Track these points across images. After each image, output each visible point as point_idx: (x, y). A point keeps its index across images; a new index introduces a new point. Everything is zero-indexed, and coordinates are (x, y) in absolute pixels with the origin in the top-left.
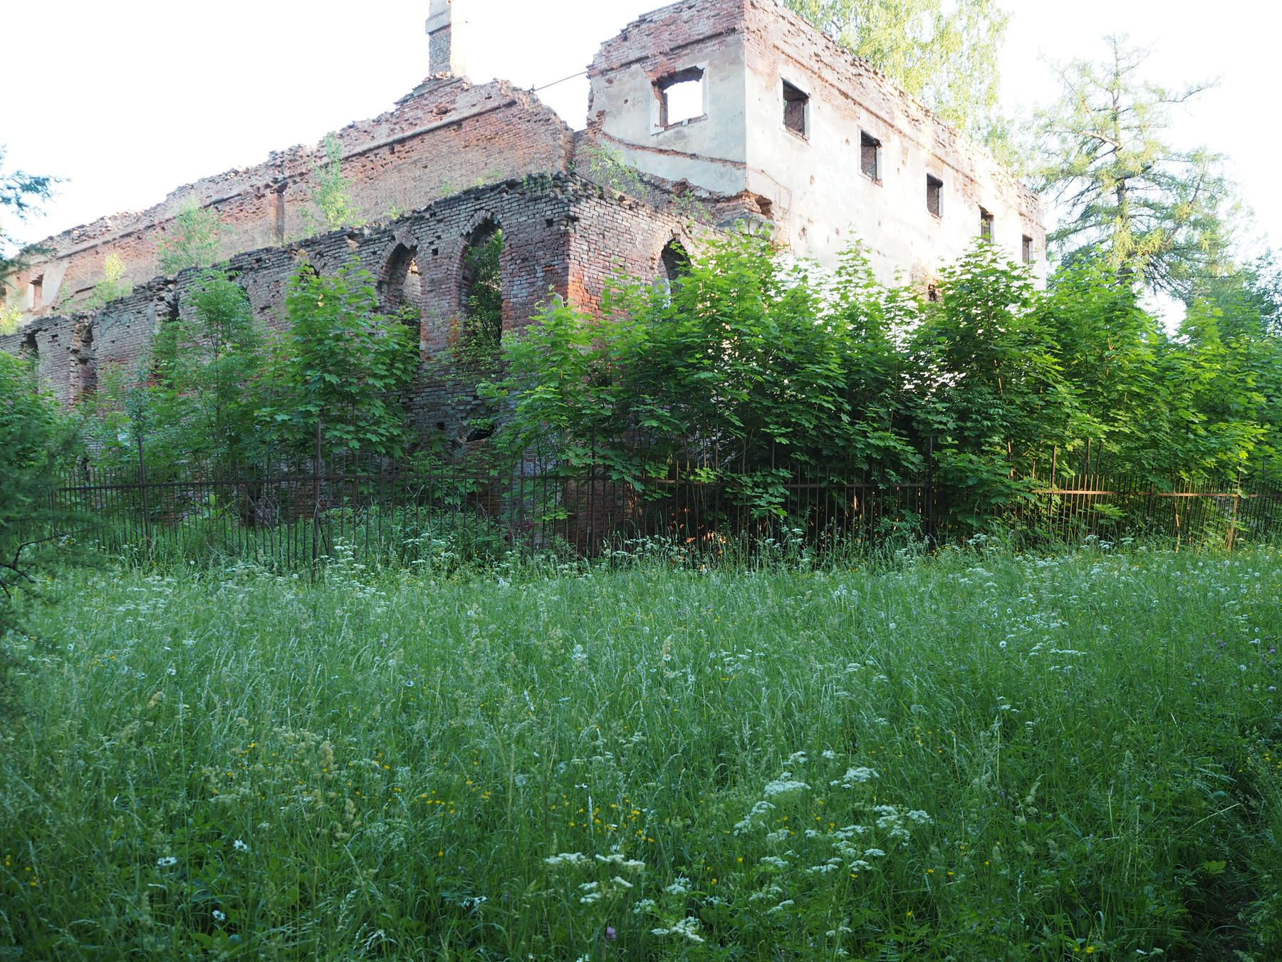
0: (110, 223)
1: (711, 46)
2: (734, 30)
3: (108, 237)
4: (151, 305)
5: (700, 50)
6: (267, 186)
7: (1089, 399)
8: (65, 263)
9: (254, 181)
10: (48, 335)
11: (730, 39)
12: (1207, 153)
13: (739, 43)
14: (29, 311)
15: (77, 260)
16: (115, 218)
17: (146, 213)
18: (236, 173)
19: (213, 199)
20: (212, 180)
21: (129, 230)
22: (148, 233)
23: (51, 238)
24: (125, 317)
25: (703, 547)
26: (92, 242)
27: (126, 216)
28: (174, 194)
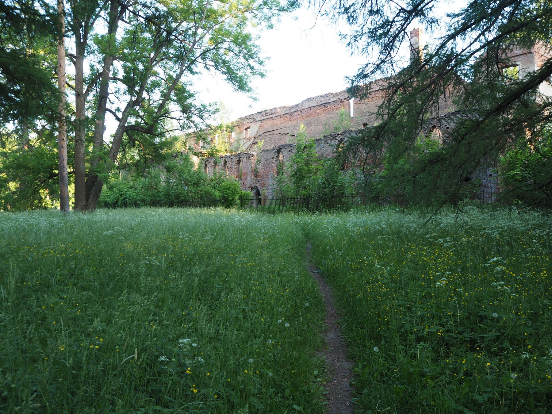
0: (278, 110)
1: (521, 58)
2: (531, 53)
3: (277, 114)
4: (333, 141)
5: (518, 59)
6: (345, 99)
7: (513, 169)
8: (260, 123)
9: (340, 97)
10: (287, 150)
11: (529, 55)
12: (349, 30)
13: (533, 57)
14: (244, 138)
15: (264, 122)
16: (280, 108)
17: (293, 107)
18: (332, 94)
19: (323, 102)
20: (322, 96)
21: (287, 112)
22: (295, 113)
23: (253, 114)
24: (322, 145)
25: (364, 227)
26: (271, 116)
27: (284, 107)
28: (306, 101)
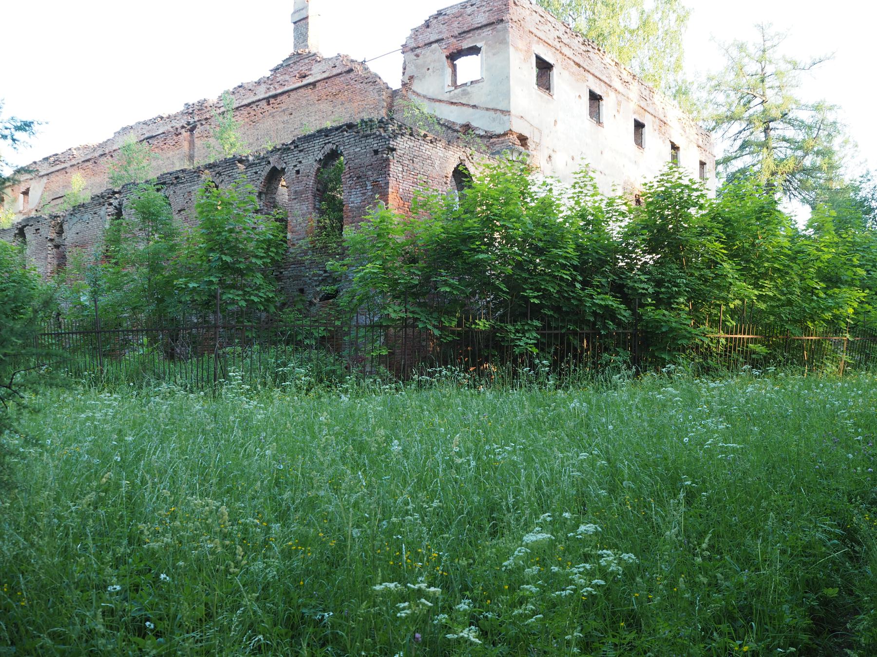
0: (75, 152)
1: (487, 32)
2: (502, 21)
3: (74, 162)
4: (104, 208)
5: (479, 34)
6: (183, 127)
7: (745, 272)
8: (45, 180)
9: (174, 123)
10: (33, 229)
11: (500, 26)
12: (826, 104)
13: (505, 30)
14: (20, 212)
15: (53, 178)
16: (79, 149)
17: (100, 145)
18: (162, 118)
19: (146, 136)
20: (145, 123)
21: (88, 157)
22: (101, 159)
23: (35, 163)
24: (86, 216)
25: (481, 374)
26: (63, 166)
27: (86, 147)
28: (119, 133)
